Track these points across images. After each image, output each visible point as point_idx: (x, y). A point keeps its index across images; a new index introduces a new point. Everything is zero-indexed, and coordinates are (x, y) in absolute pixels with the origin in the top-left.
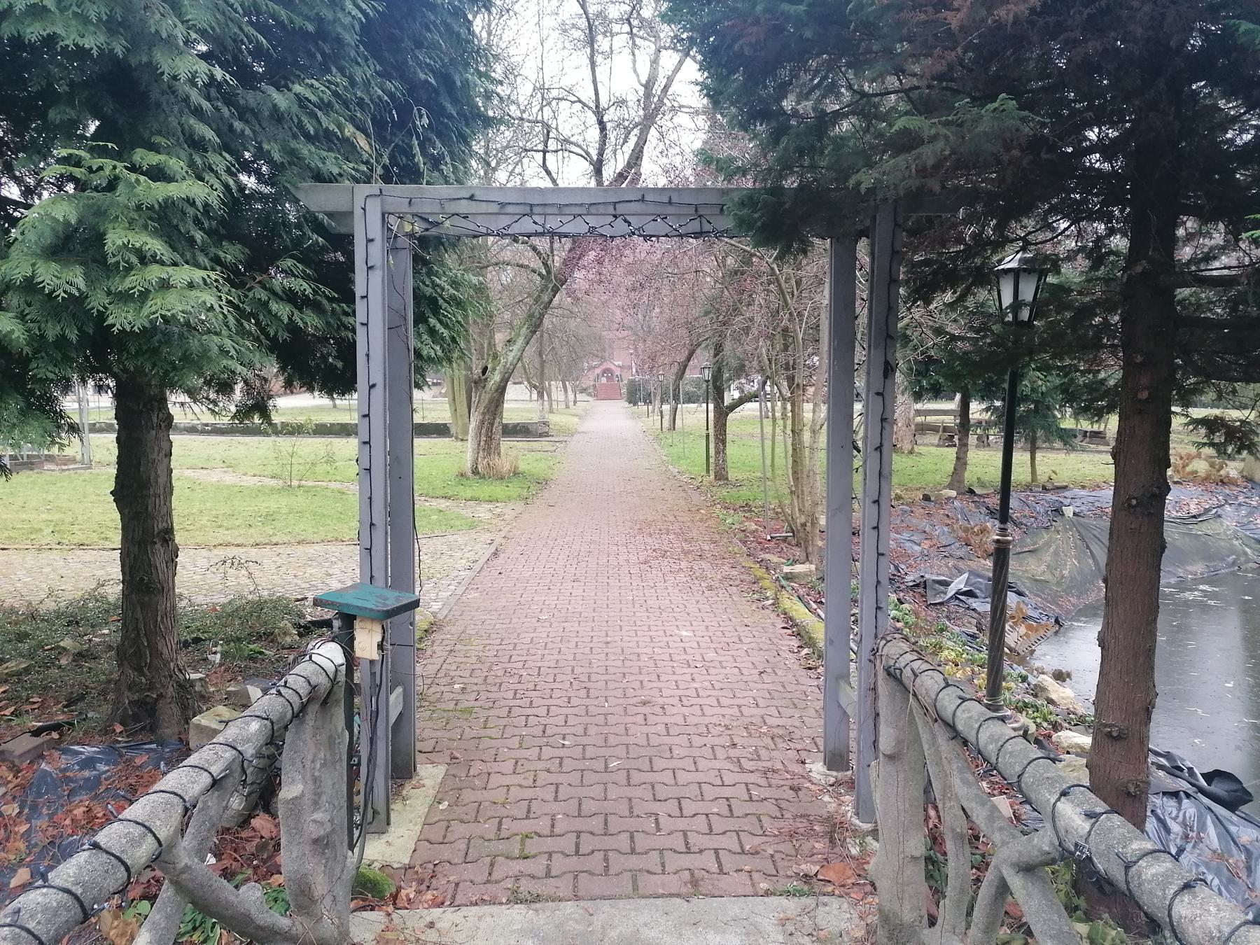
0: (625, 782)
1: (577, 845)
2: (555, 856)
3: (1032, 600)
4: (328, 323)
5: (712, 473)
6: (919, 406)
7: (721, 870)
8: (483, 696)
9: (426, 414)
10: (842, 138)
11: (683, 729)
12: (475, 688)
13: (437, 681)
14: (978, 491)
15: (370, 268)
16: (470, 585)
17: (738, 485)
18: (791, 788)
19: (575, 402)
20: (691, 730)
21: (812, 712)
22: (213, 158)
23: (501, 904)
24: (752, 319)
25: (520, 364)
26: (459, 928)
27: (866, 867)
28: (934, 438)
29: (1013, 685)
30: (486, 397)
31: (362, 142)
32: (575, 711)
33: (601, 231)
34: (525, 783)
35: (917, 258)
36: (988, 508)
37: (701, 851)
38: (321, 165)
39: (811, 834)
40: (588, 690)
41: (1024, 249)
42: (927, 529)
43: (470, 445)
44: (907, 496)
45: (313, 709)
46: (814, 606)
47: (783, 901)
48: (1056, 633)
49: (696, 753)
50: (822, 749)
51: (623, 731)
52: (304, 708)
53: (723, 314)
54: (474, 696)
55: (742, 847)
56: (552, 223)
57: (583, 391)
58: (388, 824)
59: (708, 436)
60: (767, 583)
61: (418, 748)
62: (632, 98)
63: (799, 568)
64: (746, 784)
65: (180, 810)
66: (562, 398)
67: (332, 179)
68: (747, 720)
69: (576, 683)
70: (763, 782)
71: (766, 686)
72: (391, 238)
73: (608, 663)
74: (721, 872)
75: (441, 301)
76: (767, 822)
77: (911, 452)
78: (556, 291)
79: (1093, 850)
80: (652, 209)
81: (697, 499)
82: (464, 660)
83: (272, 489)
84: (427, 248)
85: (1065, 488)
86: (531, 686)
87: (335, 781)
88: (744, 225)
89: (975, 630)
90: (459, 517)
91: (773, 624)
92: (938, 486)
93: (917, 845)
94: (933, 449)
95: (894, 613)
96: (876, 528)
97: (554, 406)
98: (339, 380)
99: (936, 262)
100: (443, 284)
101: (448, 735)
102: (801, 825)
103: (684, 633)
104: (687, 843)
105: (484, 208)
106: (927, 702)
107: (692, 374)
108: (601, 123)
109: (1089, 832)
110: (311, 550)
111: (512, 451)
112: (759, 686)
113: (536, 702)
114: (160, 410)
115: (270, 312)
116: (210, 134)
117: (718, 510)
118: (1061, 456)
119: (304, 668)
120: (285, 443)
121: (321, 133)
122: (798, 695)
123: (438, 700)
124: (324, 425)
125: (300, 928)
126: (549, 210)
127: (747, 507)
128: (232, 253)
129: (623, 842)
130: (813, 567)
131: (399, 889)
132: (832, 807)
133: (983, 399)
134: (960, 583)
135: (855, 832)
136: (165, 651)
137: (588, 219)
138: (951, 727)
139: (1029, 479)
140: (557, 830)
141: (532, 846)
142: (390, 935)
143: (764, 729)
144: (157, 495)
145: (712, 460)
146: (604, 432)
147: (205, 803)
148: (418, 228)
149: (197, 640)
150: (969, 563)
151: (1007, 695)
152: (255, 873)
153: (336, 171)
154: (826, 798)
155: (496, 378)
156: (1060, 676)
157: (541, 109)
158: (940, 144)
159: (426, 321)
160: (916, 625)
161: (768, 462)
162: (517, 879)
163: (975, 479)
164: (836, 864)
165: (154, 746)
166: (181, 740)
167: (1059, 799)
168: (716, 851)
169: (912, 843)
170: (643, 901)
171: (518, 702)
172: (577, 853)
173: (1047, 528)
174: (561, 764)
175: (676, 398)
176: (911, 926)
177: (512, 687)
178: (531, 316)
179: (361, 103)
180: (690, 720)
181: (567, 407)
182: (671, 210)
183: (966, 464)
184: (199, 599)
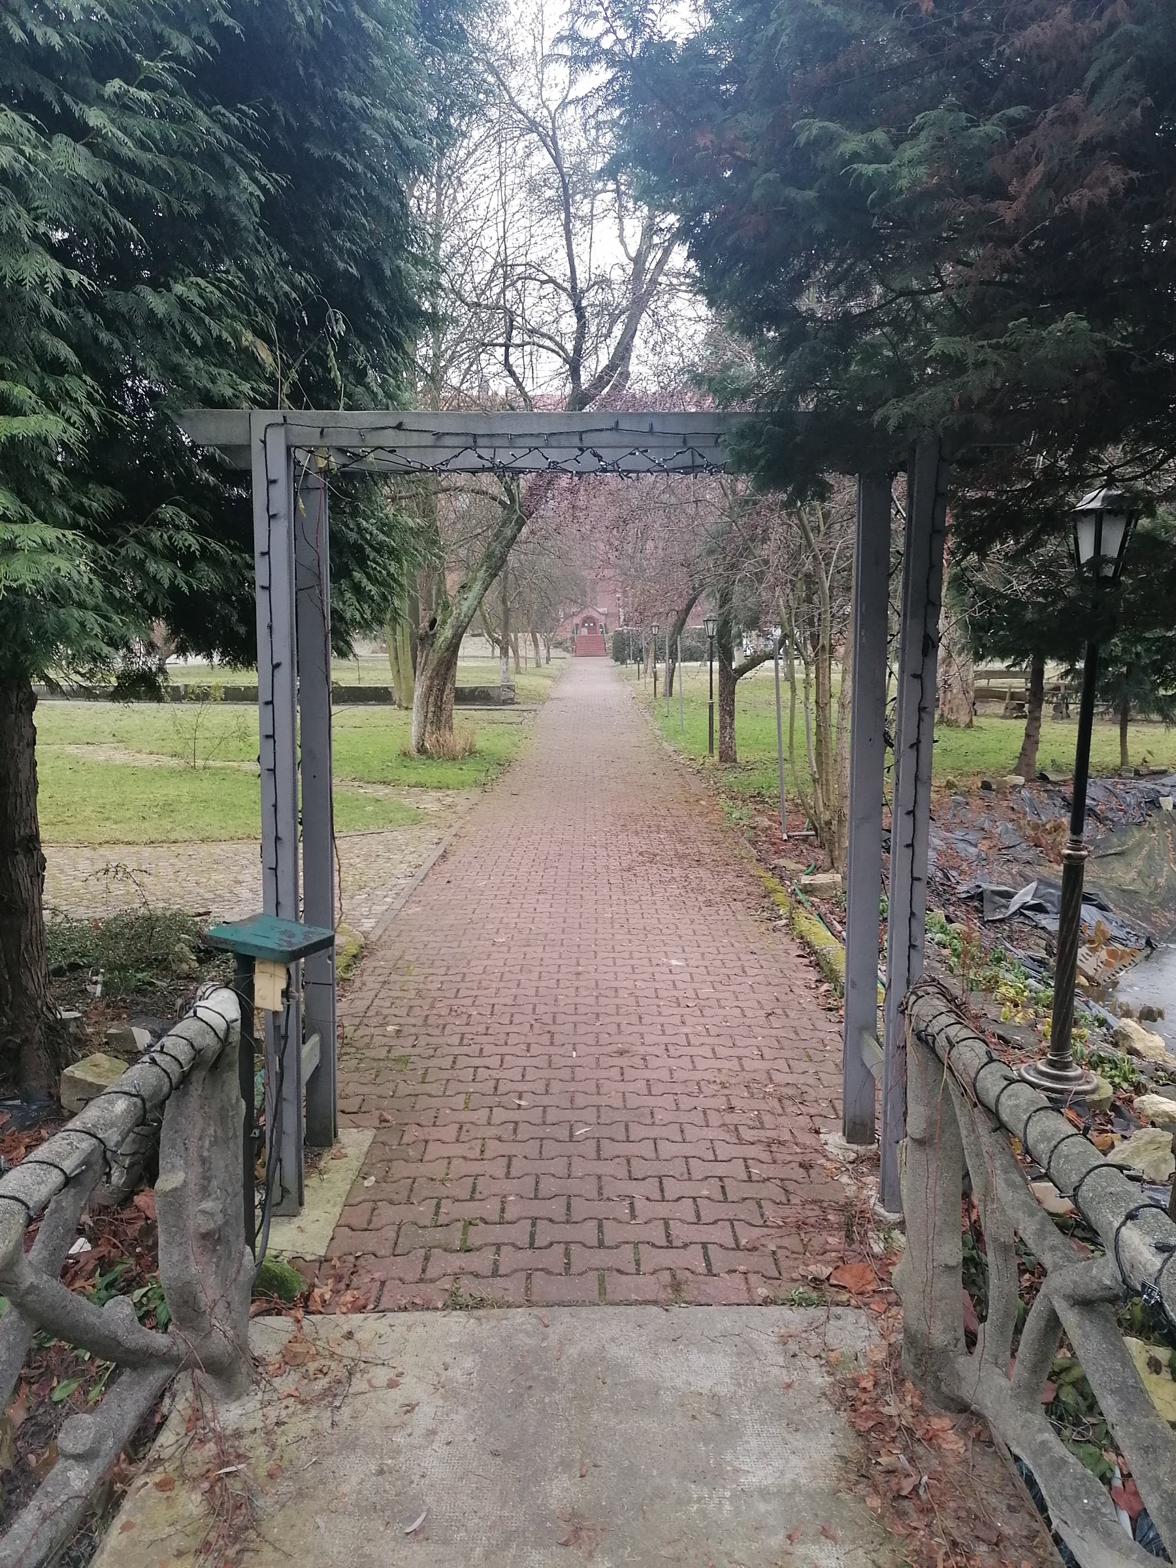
0: (594, 1155)
1: (532, 1236)
2: (504, 1249)
3: (1117, 915)
4: (227, 579)
5: (716, 752)
6: (983, 666)
7: (710, 1270)
8: (423, 1041)
9: (363, 674)
10: (872, 346)
11: (669, 1088)
12: (413, 1030)
13: (366, 1021)
14: (1052, 777)
15: (272, 517)
16: (411, 897)
17: (749, 768)
18: (801, 1165)
19: (548, 659)
20: (678, 1088)
21: (830, 1067)
22: (71, 383)
23: (437, 1309)
24: (766, 562)
25: (478, 613)
26: (382, 1340)
27: (891, 1268)
28: (999, 708)
29: (1086, 1032)
30: (434, 658)
31: (264, 353)
32: (535, 1062)
33: (563, 466)
34: (470, 1155)
35: (972, 494)
36: (1064, 799)
37: (685, 1246)
38: (210, 386)
39: (822, 1225)
40: (552, 1034)
41: (1109, 485)
42: (986, 826)
43: (415, 716)
44: (962, 783)
45: (199, 1076)
46: (839, 928)
47: (786, 1312)
48: (1147, 957)
49: (684, 1117)
50: (841, 1114)
51: (594, 1090)
52: (185, 1078)
53: (734, 549)
54: (410, 1041)
55: (736, 1240)
56: (504, 457)
57: (559, 645)
58: (301, 1204)
59: (711, 707)
60: (779, 897)
61: (339, 1107)
62: (617, 275)
63: (821, 879)
64: (745, 1160)
65: (21, 1219)
66: (531, 654)
67: (224, 404)
68: (749, 1077)
69: (537, 1026)
70: (765, 1156)
71: (774, 1032)
72: (300, 482)
73: (578, 1000)
74: (710, 1273)
75: (368, 550)
76: (769, 1209)
77: (969, 725)
78: (521, 524)
79: (1165, 1293)
80: (627, 439)
81: (697, 786)
82: (400, 994)
83: (172, 771)
84: (348, 487)
85: (1163, 773)
86: (481, 1029)
87: (229, 1163)
88: (741, 463)
89: (1043, 954)
90: (400, 808)
91: (786, 952)
92: (1002, 770)
93: (952, 1251)
94: (997, 722)
95: (939, 937)
96: (911, 846)
97: (522, 665)
98: (242, 651)
99: (994, 502)
100: (370, 527)
101: (379, 1090)
102: (812, 1213)
103: (674, 962)
104: (668, 1235)
105: (415, 439)
106: (966, 1080)
107: (694, 625)
108: (579, 311)
109: (1161, 1270)
110: (216, 849)
111: (467, 722)
112: (765, 1032)
113: (488, 1049)
114: (20, 688)
115: (147, 573)
116: (65, 352)
117: (723, 801)
118: (1160, 730)
119: (186, 1027)
120: (185, 711)
121: (212, 342)
122: (814, 1043)
123: (368, 1046)
124: (237, 689)
125: (183, 1347)
126: (497, 442)
127: (758, 798)
128: (99, 499)
129: (588, 1233)
130: (838, 878)
131: (313, 1286)
132: (851, 1191)
133: (1061, 659)
134: (1025, 894)
135: (879, 1224)
136: (31, 985)
137: (546, 452)
138: (992, 1113)
139: (1118, 761)
140: (508, 1216)
141: (476, 1236)
142: (298, 1348)
143: (770, 1088)
144: (18, 795)
145: (716, 736)
146: (582, 696)
147: (58, 1202)
148: (335, 461)
149: (74, 967)
150: (1038, 868)
151: (1079, 1046)
152: (138, 1264)
153: (229, 392)
154: (845, 1179)
155: (447, 632)
156: (1149, 1016)
157: (503, 291)
158: (990, 373)
159: (348, 574)
160: (966, 952)
161: (786, 739)
162: (456, 1277)
163: (1048, 762)
164: (855, 1266)
165: (18, 1102)
166: (50, 1095)
167: (1124, 1224)
168: (704, 1245)
169: (946, 1249)
170: (610, 1310)
171: (465, 1050)
172: (531, 1245)
173: (1139, 824)
174: (515, 1130)
175: (673, 656)
176: (944, 1351)
177: (458, 1029)
178: (489, 556)
179: (261, 301)
180: (679, 1075)
181: (538, 666)
182: (652, 441)
183: (1037, 743)
184: (81, 913)
